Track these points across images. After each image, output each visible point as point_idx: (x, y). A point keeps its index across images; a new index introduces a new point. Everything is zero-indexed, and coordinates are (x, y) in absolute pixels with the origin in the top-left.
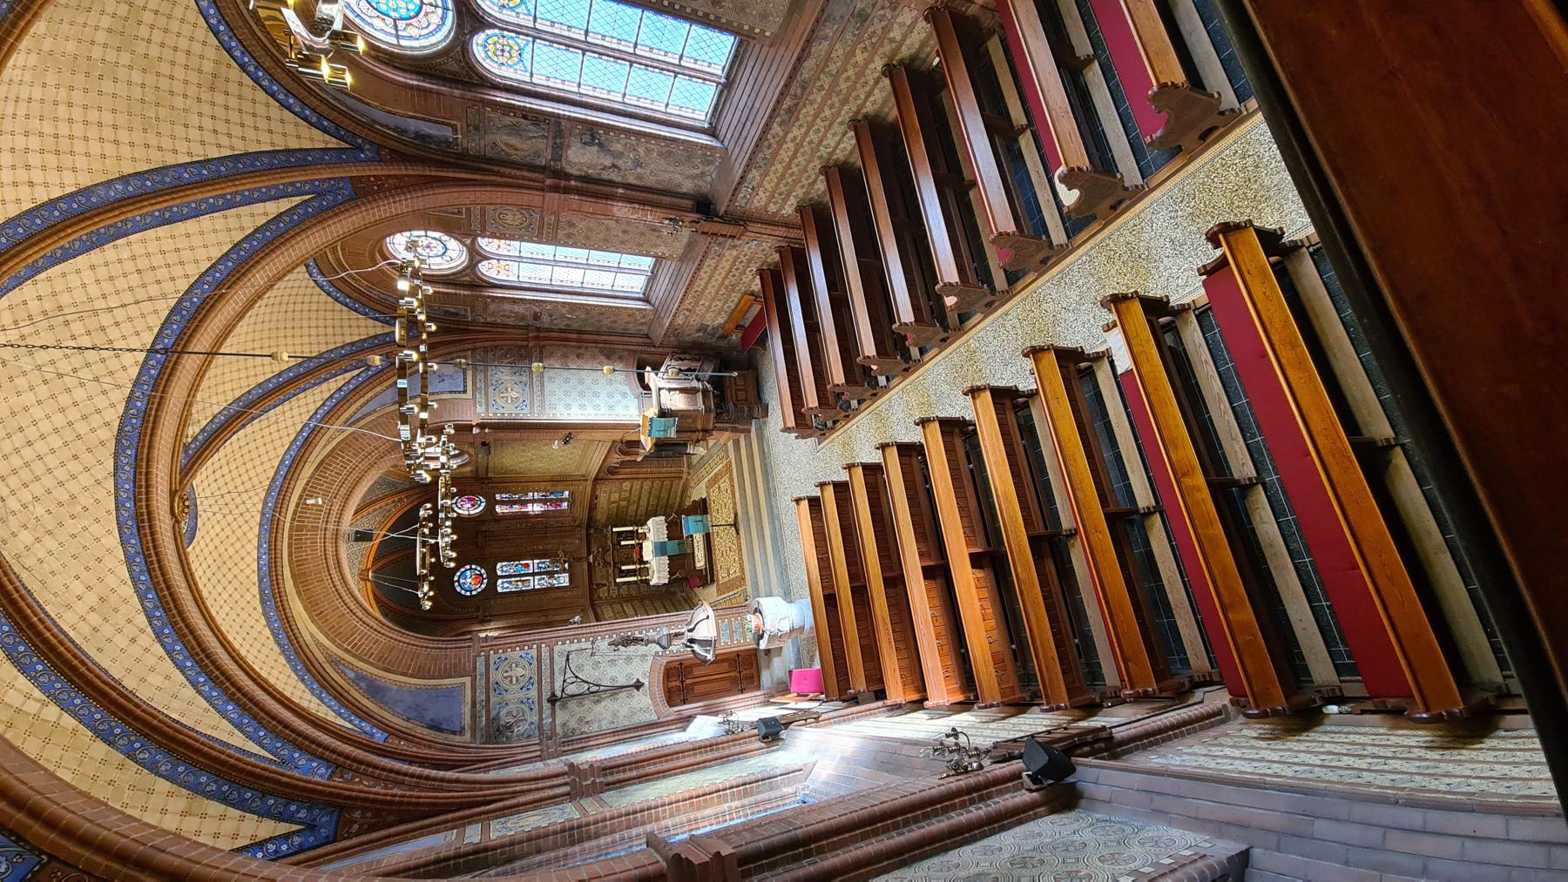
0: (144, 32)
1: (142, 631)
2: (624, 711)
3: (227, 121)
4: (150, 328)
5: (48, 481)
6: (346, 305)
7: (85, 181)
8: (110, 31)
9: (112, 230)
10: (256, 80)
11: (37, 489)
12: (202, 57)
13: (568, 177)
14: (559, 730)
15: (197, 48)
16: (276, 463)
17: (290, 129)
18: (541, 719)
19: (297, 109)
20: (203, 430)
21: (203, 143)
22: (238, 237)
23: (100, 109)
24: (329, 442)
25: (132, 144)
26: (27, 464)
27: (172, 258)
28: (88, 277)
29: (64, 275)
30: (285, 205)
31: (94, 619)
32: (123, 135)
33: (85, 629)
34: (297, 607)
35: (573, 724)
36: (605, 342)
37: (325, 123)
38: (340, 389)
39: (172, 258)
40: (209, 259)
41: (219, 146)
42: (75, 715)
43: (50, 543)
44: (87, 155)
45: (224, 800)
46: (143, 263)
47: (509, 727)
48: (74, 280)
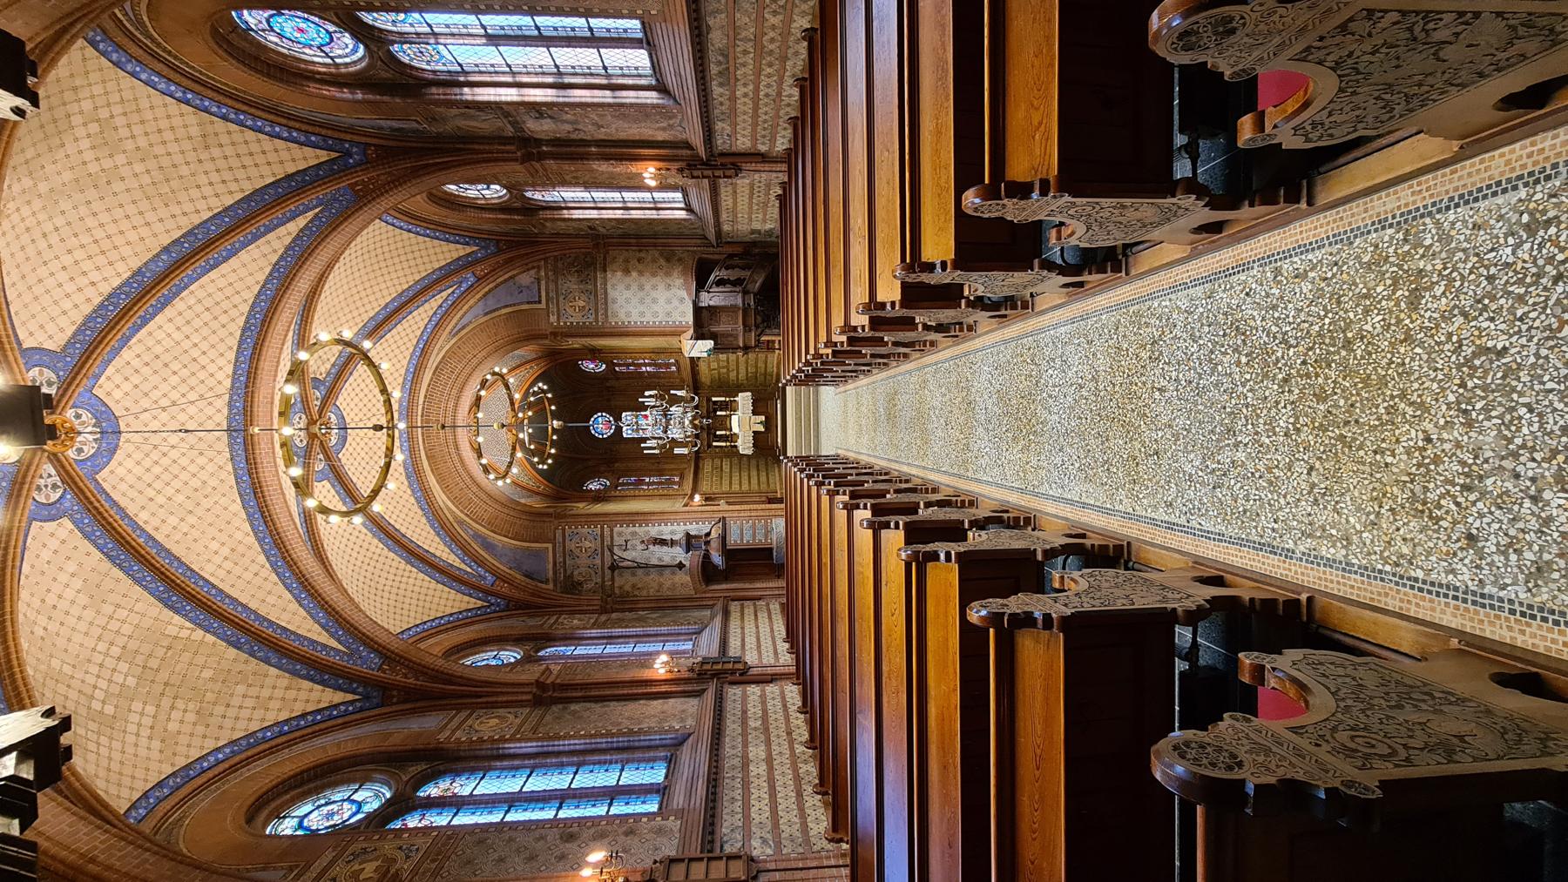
0: (124, 132)
1: (263, 566)
2: (668, 584)
3: (231, 169)
4: (231, 348)
5: (184, 476)
6: (428, 236)
7: (136, 263)
8: (92, 148)
9: (174, 289)
10: (241, 124)
11: (177, 484)
12: (186, 126)
13: (539, 142)
14: (617, 591)
15: (177, 121)
16: (403, 371)
17: (285, 155)
18: (603, 582)
19: (285, 135)
20: (333, 365)
21: (217, 195)
22: (274, 258)
23: (121, 206)
24: (440, 350)
25: (161, 220)
26: (166, 470)
27: (229, 291)
28: (169, 328)
29: (150, 334)
30: (301, 222)
31: (228, 565)
32: (151, 217)
33: (222, 573)
34: (432, 480)
35: (627, 588)
36: (664, 245)
37: (313, 138)
38: (441, 306)
39: (229, 291)
40: (257, 283)
41: (231, 193)
42: (214, 634)
43: (191, 520)
44: (128, 243)
45: (312, 680)
46: (208, 303)
47: (580, 584)
48: (160, 335)
